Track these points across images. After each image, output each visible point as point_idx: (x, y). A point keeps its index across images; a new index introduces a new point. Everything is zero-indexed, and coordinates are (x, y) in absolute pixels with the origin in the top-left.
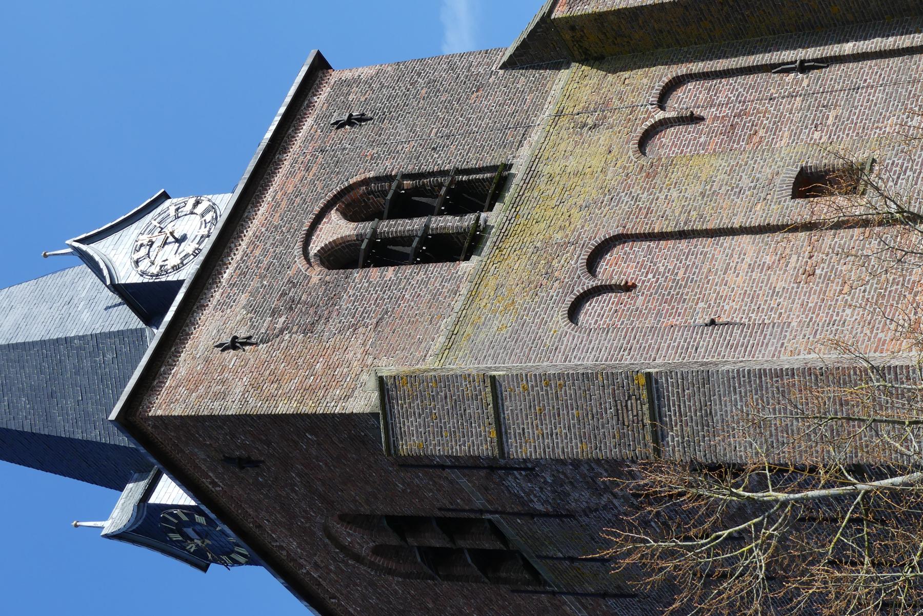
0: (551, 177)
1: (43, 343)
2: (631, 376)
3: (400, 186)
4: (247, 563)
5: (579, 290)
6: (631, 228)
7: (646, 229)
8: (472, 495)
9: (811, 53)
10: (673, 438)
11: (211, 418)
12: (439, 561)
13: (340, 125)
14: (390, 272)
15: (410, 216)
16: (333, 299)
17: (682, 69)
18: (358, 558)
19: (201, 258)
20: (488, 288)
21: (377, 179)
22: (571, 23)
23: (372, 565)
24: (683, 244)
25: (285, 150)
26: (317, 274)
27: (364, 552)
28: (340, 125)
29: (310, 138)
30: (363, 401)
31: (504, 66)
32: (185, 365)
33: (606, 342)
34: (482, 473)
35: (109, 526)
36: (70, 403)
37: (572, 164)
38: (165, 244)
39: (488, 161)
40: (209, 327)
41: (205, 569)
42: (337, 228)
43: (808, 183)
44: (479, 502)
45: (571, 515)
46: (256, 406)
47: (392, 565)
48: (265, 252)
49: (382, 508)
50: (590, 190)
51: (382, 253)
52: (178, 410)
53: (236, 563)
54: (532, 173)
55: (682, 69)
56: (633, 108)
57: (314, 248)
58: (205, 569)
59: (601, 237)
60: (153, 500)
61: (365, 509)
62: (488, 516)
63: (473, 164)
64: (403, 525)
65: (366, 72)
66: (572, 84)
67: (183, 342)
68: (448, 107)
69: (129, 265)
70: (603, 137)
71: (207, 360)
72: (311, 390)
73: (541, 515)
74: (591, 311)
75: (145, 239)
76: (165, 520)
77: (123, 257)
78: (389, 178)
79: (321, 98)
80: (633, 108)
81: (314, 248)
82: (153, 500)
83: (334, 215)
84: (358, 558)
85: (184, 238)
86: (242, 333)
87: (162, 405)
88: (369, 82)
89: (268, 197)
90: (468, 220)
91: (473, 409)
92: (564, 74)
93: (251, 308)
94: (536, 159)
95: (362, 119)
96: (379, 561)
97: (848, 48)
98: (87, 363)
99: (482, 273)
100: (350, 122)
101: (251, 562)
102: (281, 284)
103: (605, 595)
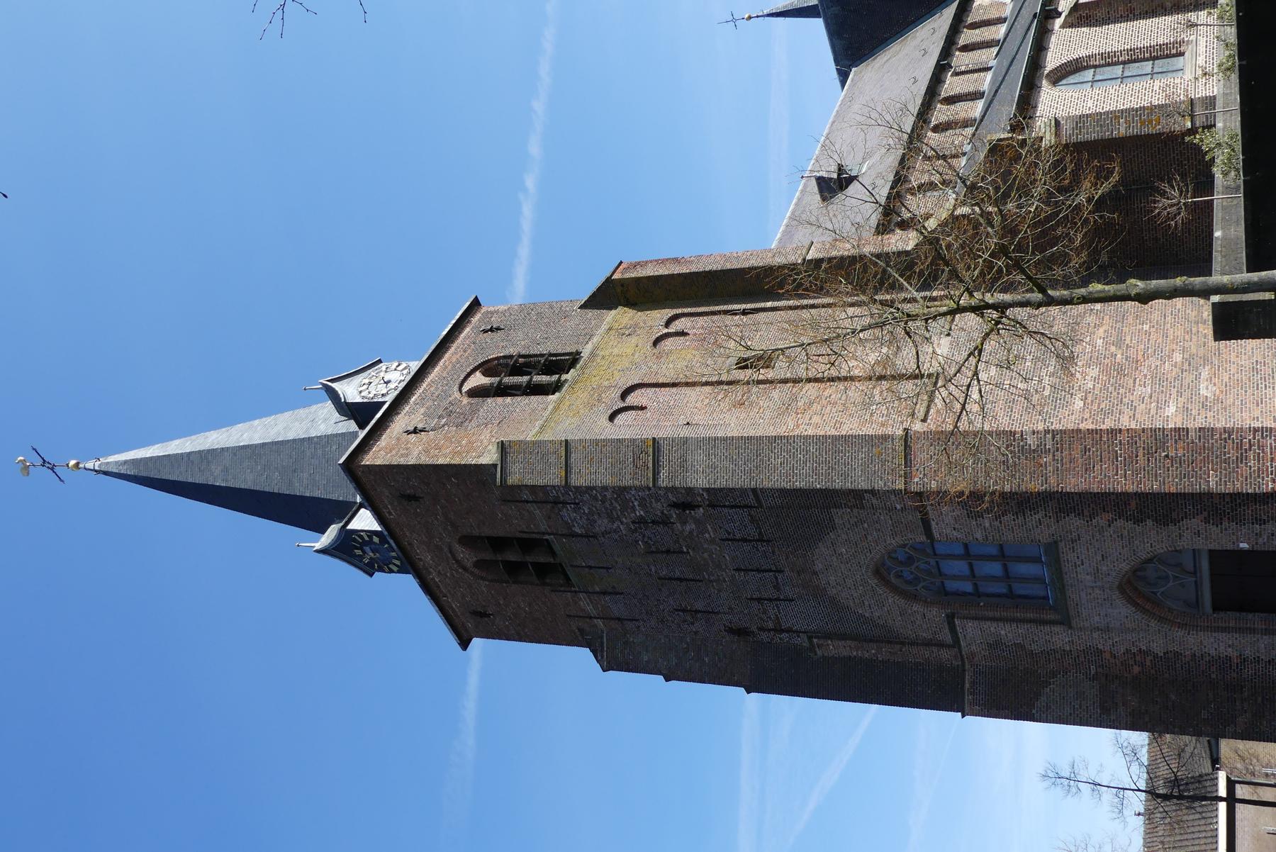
0: (603, 357)
1: (294, 440)
2: (644, 441)
3: (516, 361)
4: (399, 572)
5: (615, 408)
6: (646, 381)
7: (655, 381)
8: (539, 522)
9: (749, 306)
10: (663, 474)
11: (398, 466)
12: (514, 570)
13: (485, 331)
14: (509, 399)
15: (522, 375)
16: (474, 411)
17: (679, 311)
18: (465, 569)
19: (397, 392)
20: (564, 407)
21: (504, 357)
22: (622, 282)
23: (472, 573)
24: (674, 390)
25: (453, 342)
26: (465, 400)
27: (469, 564)
28: (485, 331)
29: (468, 337)
30: (489, 457)
31: (581, 307)
32: (385, 440)
33: (628, 428)
34: (549, 506)
35: (318, 546)
36: (306, 475)
37: (616, 351)
38: (380, 385)
39: (568, 350)
40: (400, 423)
41: (371, 575)
42: (479, 380)
43: (743, 364)
44: (543, 528)
45: (595, 536)
46: (425, 460)
47: (484, 574)
48: (437, 389)
49: (487, 531)
50: (626, 363)
51: (502, 391)
52: (378, 462)
53: (391, 571)
54: (593, 355)
55: (679, 311)
56: (651, 327)
57: (465, 389)
58: (371, 575)
59: (630, 384)
60: (349, 527)
61: (476, 532)
62: (547, 537)
63: (560, 351)
64: (498, 543)
65: (502, 308)
66: (621, 316)
67: (385, 430)
68: (548, 324)
69: (356, 393)
70: (634, 340)
71: (398, 439)
72: (459, 453)
73: (577, 535)
74: (621, 418)
75: (367, 381)
76: (355, 540)
77: (351, 391)
78: (511, 357)
79: (475, 319)
80: (651, 327)
81: (465, 389)
82: (349, 527)
83: (478, 374)
84: (465, 569)
85: (389, 382)
86: (420, 426)
87: (368, 460)
88: (504, 313)
89: (441, 363)
90: (555, 377)
91: (552, 459)
92: (613, 312)
93: (425, 414)
94: (596, 348)
95: (498, 329)
96: (476, 571)
97: (769, 304)
98: (320, 452)
99: (560, 401)
100: (491, 330)
101: (402, 570)
102: (445, 404)
103: (604, 593)
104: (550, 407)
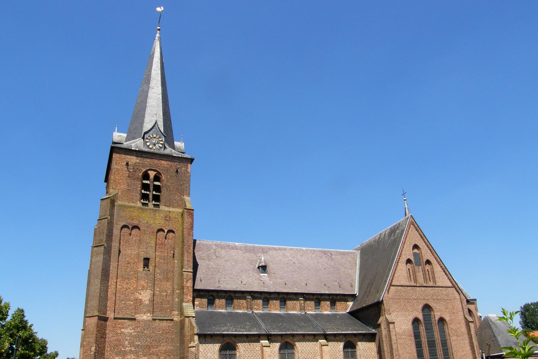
42: (152, 174)
104: (133, 205)
